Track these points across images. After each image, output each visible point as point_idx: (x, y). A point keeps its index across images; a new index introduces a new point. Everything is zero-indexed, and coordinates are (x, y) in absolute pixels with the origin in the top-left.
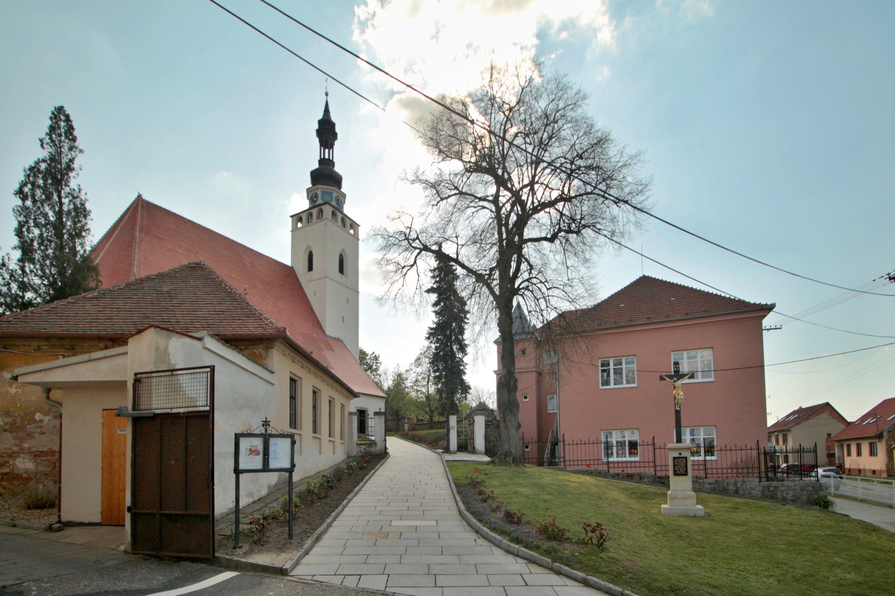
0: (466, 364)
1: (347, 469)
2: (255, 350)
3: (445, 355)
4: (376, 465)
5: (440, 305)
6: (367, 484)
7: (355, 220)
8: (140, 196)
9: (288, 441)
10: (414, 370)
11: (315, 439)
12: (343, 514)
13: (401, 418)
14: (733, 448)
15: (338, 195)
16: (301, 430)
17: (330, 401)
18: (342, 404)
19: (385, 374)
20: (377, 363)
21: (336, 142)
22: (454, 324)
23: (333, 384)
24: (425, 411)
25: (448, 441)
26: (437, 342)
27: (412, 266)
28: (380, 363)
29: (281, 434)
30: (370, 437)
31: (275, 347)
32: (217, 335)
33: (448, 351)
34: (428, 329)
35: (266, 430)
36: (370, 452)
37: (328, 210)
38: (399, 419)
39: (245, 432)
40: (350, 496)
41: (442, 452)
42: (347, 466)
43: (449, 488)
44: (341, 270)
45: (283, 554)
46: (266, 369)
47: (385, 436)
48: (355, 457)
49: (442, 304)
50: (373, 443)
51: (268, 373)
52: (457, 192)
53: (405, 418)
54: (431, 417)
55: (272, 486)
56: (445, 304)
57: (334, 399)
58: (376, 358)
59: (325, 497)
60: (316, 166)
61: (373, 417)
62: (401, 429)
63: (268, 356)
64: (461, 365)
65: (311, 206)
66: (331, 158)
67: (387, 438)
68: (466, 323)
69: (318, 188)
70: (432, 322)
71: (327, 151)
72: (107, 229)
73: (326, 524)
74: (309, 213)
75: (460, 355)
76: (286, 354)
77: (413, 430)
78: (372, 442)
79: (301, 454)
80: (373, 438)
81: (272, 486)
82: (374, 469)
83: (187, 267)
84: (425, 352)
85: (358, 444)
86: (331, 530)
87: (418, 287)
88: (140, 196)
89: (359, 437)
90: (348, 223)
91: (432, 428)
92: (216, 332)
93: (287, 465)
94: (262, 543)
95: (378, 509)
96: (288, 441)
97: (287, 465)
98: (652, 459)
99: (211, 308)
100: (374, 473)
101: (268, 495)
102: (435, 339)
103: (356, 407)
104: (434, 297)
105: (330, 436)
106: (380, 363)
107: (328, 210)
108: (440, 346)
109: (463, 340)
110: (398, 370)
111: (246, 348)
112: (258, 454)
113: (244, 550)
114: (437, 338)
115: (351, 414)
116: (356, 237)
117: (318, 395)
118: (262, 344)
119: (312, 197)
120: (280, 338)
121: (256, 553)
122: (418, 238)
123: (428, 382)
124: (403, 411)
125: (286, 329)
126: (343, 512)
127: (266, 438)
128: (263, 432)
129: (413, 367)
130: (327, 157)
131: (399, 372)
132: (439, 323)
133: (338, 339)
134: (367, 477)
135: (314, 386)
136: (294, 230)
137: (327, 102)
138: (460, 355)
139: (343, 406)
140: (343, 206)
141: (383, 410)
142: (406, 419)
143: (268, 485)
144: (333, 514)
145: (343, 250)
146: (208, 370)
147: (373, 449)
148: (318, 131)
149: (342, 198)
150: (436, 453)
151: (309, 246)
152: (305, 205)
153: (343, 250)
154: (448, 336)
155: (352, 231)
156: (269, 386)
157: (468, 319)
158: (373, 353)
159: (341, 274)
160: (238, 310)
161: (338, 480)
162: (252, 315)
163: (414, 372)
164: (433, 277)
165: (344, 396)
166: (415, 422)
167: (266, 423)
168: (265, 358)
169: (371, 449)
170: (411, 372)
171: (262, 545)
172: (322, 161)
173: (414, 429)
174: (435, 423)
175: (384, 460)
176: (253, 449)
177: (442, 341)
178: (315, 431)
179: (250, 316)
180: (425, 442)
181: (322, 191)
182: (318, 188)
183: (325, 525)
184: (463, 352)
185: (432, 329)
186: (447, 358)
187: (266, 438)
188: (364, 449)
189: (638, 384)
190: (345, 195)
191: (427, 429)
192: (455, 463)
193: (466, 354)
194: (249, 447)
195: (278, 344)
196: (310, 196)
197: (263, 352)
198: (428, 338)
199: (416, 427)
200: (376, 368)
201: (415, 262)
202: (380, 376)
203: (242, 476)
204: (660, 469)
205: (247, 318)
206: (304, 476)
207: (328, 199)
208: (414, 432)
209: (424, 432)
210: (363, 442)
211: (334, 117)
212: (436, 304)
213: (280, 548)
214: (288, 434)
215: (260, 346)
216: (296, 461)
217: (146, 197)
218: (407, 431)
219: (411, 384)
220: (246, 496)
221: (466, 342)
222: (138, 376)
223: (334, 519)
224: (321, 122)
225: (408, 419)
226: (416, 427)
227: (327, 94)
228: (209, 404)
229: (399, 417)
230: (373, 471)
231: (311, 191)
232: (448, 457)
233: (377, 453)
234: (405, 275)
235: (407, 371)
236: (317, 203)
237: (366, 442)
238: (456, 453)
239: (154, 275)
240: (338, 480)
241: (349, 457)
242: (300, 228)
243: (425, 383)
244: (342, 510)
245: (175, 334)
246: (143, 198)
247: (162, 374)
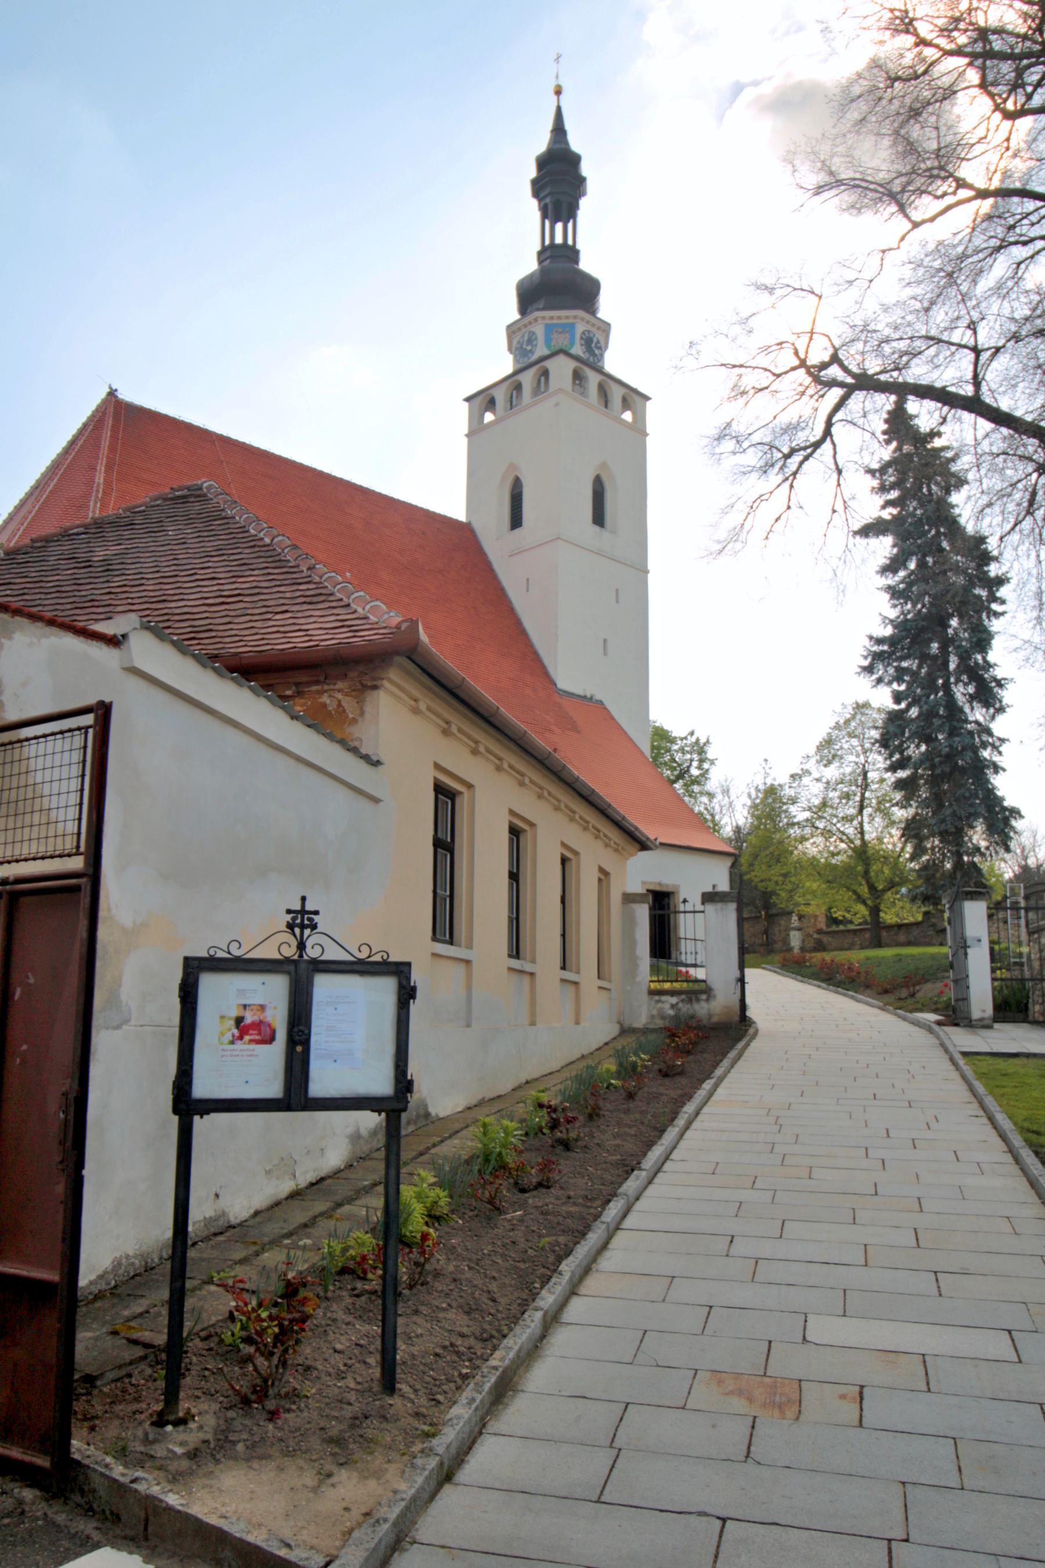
0: (1002, 740)
1: (618, 1075)
2: (325, 699)
3: (928, 716)
4: (716, 1065)
5: (906, 568)
6: (689, 1134)
7: (634, 385)
8: (112, 393)
9: (386, 988)
10: (815, 775)
11: (515, 977)
12: (608, 1262)
13: (776, 915)
15: (589, 327)
16: (469, 947)
17: (564, 861)
18: (601, 870)
19: (726, 792)
20: (702, 761)
21: (583, 202)
22: (954, 622)
23: (574, 807)
24: (855, 892)
25: (962, 982)
26: (899, 679)
27: (817, 445)
28: (712, 762)
29: (361, 962)
30: (692, 971)
31: (386, 683)
32: (214, 658)
33: (937, 703)
34: (867, 642)
35: (301, 946)
36: (692, 1017)
37: (561, 369)
38: (771, 918)
39: (221, 954)
40: (631, 1185)
41: (939, 1023)
42: (621, 1065)
43: (1015, 1169)
44: (599, 518)
45: (343, 1475)
46: (354, 750)
47: (742, 967)
48: (645, 1031)
49: (912, 566)
50: (701, 991)
51: (362, 765)
52: (972, 193)
53: (790, 913)
54: (875, 911)
55: (364, 1132)
56: (922, 564)
57: (576, 853)
58: (700, 749)
59: (540, 1185)
60: (530, 265)
61: (700, 907)
62: (777, 946)
63: (362, 713)
64: (984, 745)
65: (519, 366)
66: (570, 242)
67: (750, 973)
68: (997, 615)
69: (536, 320)
70: (879, 619)
71: (559, 226)
72: (37, 475)
73: (539, 1315)
74: (513, 384)
75: (978, 714)
76: (423, 707)
77: (816, 949)
78: (696, 987)
79: (468, 1025)
80: (700, 974)
81: (364, 1132)
82: (709, 1077)
83: (165, 499)
84: (847, 722)
85: (652, 993)
86: (560, 1339)
87: (839, 506)
88: (112, 393)
89: (655, 970)
90: (616, 394)
91: (879, 944)
92: (212, 649)
93: (382, 1085)
94: (271, 1404)
95: (740, 1247)
96: (386, 988)
97: (382, 1085)
99: (210, 588)
100: (711, 1094)
101: (350, 1166)
102: (891, 671)
103: (643, 883)
104: (884, 546)
105: (563, 968)
106: (712, 762)
107: (561, 369)
108: (908, 689)
109: (988, 666)
110: (767, 774)
111: (299, 694)
112: (270, 1039)
113: (191, 1436)
114: (898, 669)
115: (629, 899)
116: (639, 429)
117: (526, 840)
120: (397, 653)
121: (236, 1458)
122: (835, 359)
123: (861, 808)
124: (783, 894)
125: (417, 622)
126: (607, 1254)
128: (290, 951)
129: (811, 765)
131: (769, 782)
132: (906, 621)
133: (591, 698)
134: (689, 1108)
135: (512, 812)
136: (475, 431)
138: (978, 714)
139: (604, 874)
140: (602, 355)
141: (724, 886)
142: (795, 918)
143: (350, 1130)
144: (568, 1267)
145: (604, 465)
146: (88, 719)
147: (702, 1009)
148: (535, 183)
149: (599, 336)
150: (917, 1023)
151: (512, 466)
153: (604, 465)
154: (935, 658)
155: (628, 416)
156: (364, 804)
157: (1003, 602)
158: (692, 734)
159: (597, 528)
160: (282, 589)
161: (590, 1117)
162: (322, 598)
163: (818, 780)
164: (883, 489)
165: (607, 846)
166: (822, 924)
168: (354, 721)
169: (696, 1006)
170: (806, 780)
171: (273, 1415)
173: (820, 947)
174: (890, 927)
175: (740, 1045)
176: (249, 1018)
177: (915, 674)
178: (515, 952)
179: (315, 599)
180: (868, 987)
181: (547, 326)
182: (536, 320)
183: (533, 1320)
184: (987, 705)
185: (879, 641)
186: (937, 722)
188: (673, 1006)
190: (609, 325)
191: (862, 948)
192: (1001, 1064)
193: (1001, 710)
194: (235, 1013)
195: (393, 674)
196: (515, 342)
197: (349, 704)
198: (869, 669)
199: (825, 939)
200: (702, 775)
201: (827, 433)
202: (711, 796)
203: (200, 1124)
205: (305, 607)
206: (480, 1097)
207: (560, 341)
208: (828, 956)
209: (857, 956)
210: (667, 986)
211: (576, 143)
212: (891, 567)
213: (337, 1441)
214: (385, 963)
215: (340, 685)
216: (413, 1069)
217: (126, 395)
218: (796, 950)
219: (807, 815)
220: (268, 1172)
221: (999, 673)
223: (573, 1291)
224: (544, 162)
225: (801, 917)
226: (825, 939)
227: (558, 92)
228: (82, 849)
229: (773, 911)
230: (707, 1085)
231: (519, 329)
232: (962, 1039)
233: (715, 1019)
234: (795, 474)
235: (793, 776)
237: (677, 986)
238: (989, 1027)
239: (78, 527)
240: (590, 1117)
241: (625, 1031)
242: (491, 424)
243: (852, 811)
244: (604, 1246)
245: (24, 621)
246: (120, 396)
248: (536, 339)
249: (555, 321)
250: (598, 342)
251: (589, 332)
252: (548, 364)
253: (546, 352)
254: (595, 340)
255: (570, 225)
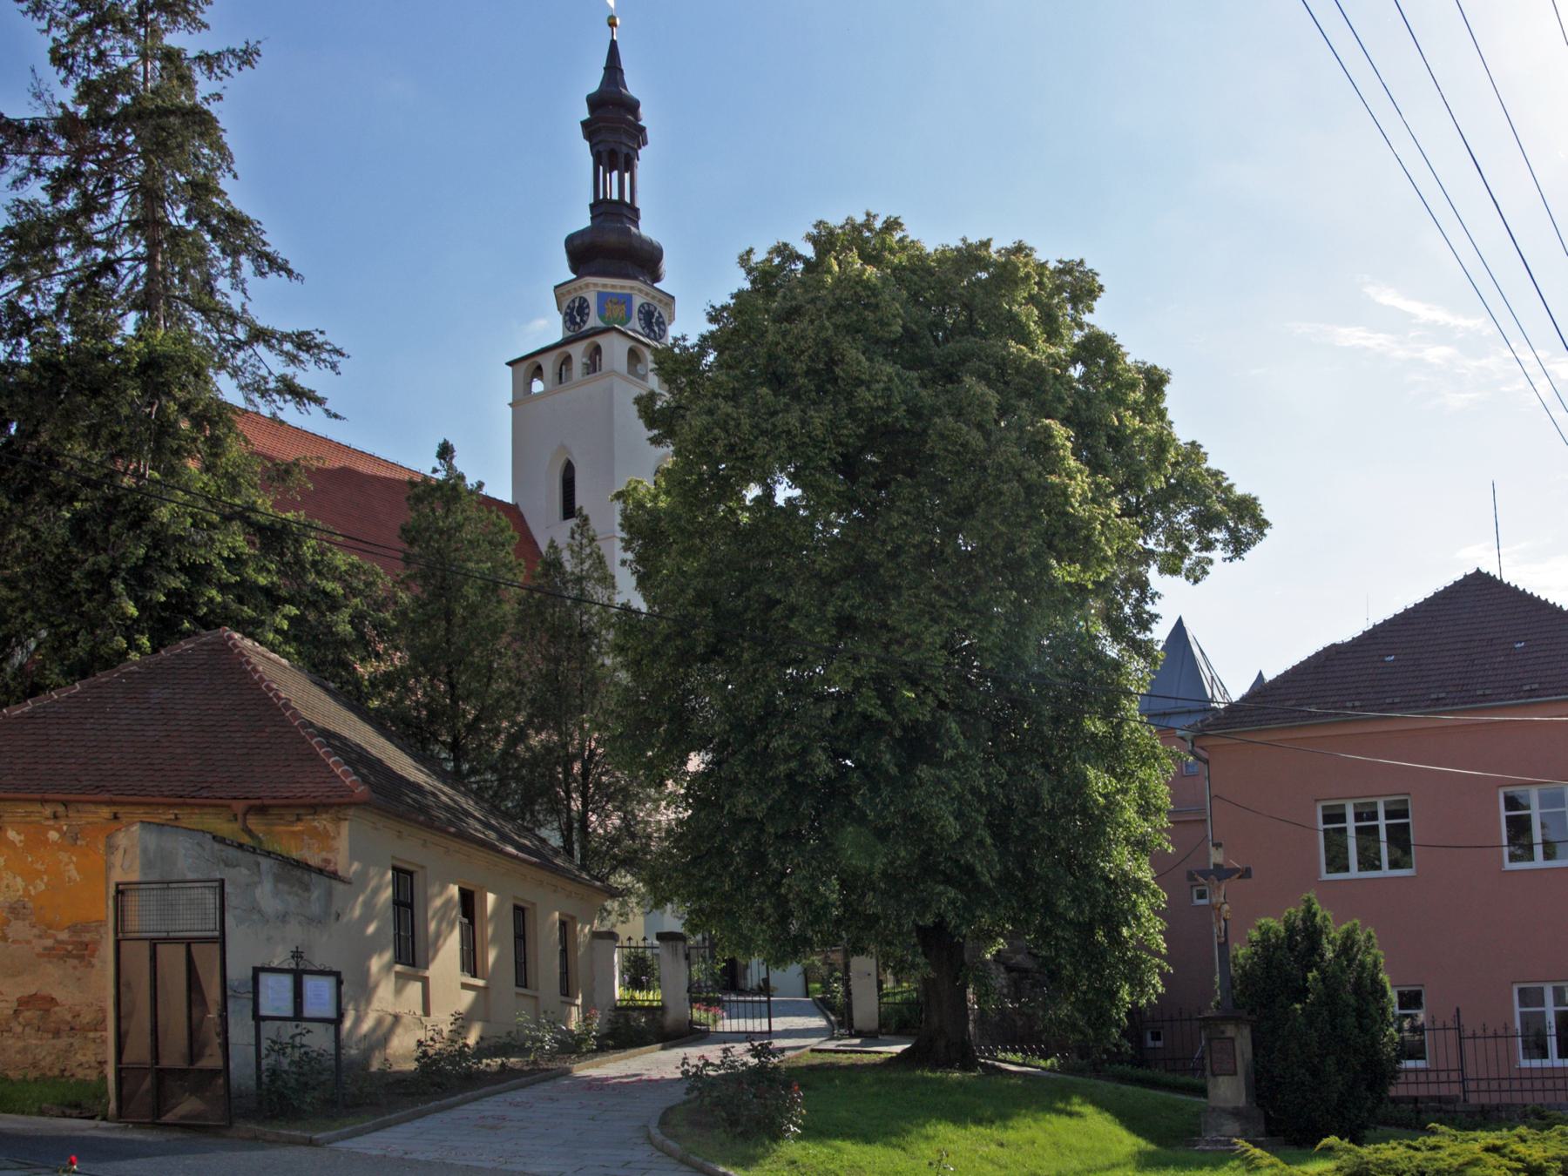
2: (316, 824)
5: (503, 1065)
14: (1479, 1033)
21: (642, 152)
60: (582, 220)
66: (627, 199)
97: (331, 1013)
98: (1454, 1065)
118: (327, 812)
119: (574, 313)
127: (298, 975)
128: (293, 966)
130: (615, 196)
137: (613, 44)
146: (217, 884)
152: (549, 328)
167: (297, 955)
168: (334, 838)
172: (601, 207)
181: (600, 295)
182: (587, 285)
187: (298, 975)
189: (1417, 871)
197: (330, 827)
203: (262, 1024)
204: (1496, 1088)
211: (634, 86)
215: (324, 816)
222: (121, 887)
224: (594, 102)
236: (587, 327)
242: (539, 394)
247: (154, 886)
248: (588, 307)
249: (609, 290)
250: (660, 316)
251: (648, 304)
252: (600, 340)
253: (600, 324)
254: (656, 314)
255: (627, 176)
